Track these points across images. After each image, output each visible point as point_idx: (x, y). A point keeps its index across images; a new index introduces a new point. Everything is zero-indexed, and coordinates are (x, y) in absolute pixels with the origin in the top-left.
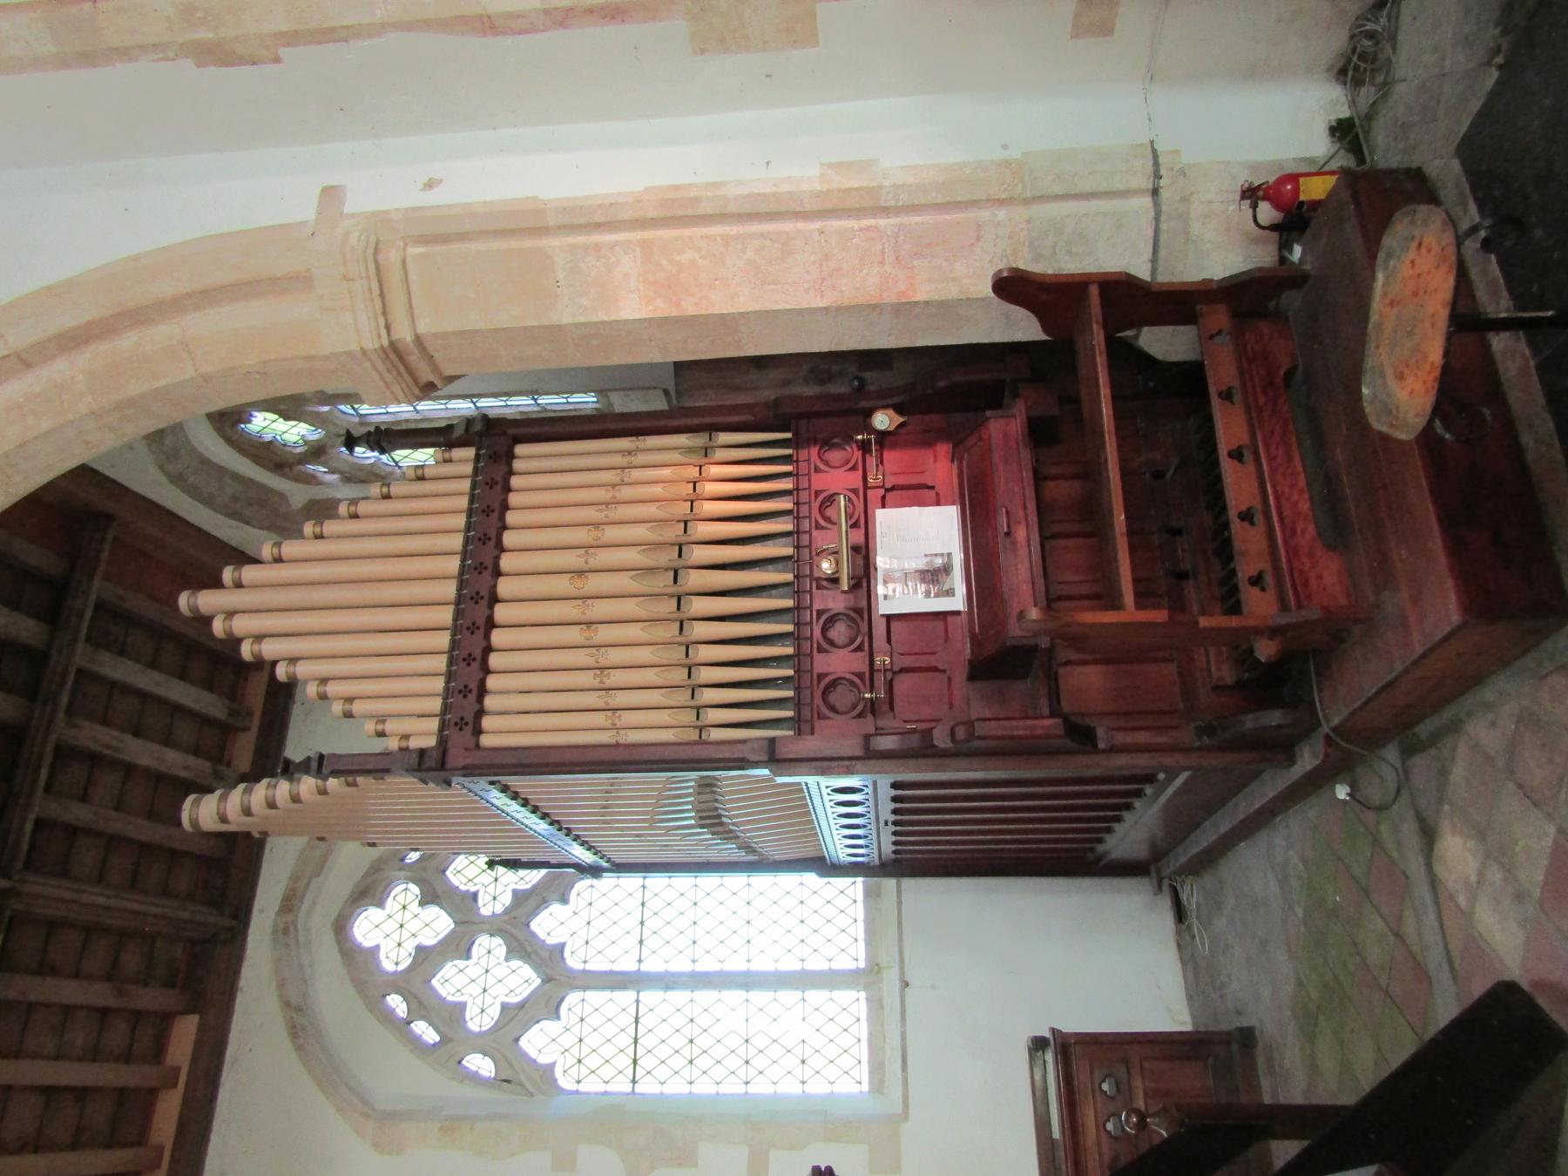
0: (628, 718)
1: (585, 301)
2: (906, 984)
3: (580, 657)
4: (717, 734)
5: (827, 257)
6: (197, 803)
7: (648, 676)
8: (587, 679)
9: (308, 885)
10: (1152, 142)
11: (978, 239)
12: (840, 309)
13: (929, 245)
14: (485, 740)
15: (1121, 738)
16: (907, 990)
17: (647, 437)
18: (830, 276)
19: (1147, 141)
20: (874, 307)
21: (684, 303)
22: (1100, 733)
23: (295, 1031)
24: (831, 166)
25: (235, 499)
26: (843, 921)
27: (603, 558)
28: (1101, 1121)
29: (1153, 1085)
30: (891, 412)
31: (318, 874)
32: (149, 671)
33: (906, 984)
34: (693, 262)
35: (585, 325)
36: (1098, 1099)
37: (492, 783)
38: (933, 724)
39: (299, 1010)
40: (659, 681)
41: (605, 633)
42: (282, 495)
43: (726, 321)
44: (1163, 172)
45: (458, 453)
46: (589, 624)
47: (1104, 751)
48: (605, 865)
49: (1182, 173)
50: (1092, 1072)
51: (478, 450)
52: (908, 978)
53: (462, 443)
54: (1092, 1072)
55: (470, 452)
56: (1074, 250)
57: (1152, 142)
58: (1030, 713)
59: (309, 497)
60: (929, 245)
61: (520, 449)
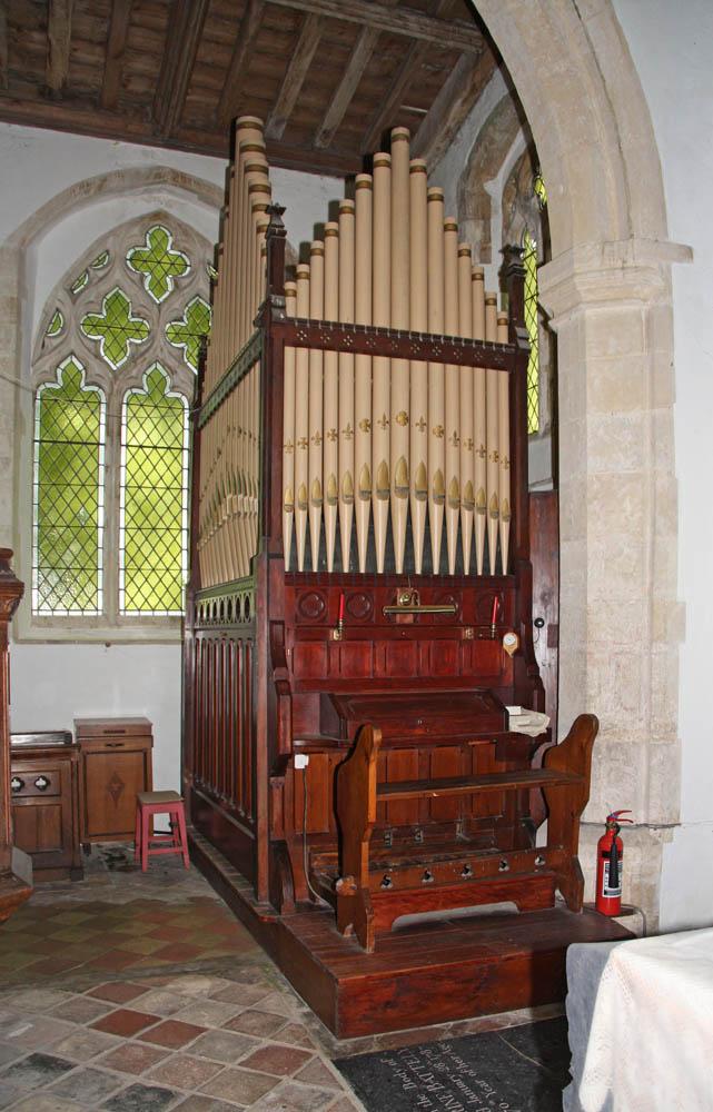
0: (301, 453)
1: (601, 432)
2: (108, 645)
3: (347, 419)
4: (287, 517)
5: (621, 605)
6: (257, 127)
7: (331, 469)
8: (331, 425)
9: (192, 191)
10: (679, 824)
11: (626, 709)
12: (586, 613)
13: (624, 677)
14: (289, 351)
15: (277, 793)
16: (104, 646)
17: (508, 470)
18: (608, 606)
19: (681, 821)
20: (585, 634)
21: (595, 502)
22: (281, 779)
23: (85, 186)
24: (683, 610)
25: (492, 141)
26: (153, 601)
27: (419, 436)
28: (19, 776)
29: (44, 811)
30: (516, 646)
31: (200, 199)
32: (361, 73)
33: (108, 645)
34: (624, 511)
35: (585, 431)
36: (33, 775)
37: (260, 353)
38: (290, 668)
39: (100, 187)
40: (327, 476)
41: (363, 437)
42: (494, 175)
43: (582, 535)
44: (658, 831)
45: (504, 330)
46: (371, 426)
47: (269, 780)
48: (201, 423)
49: (656, 843)
50: (52, 771)
51: (506, 346)
52: (112, 647)
53: (512, 335)
54: (52, 771)
55: (504, 340)
56: (613, 773)
57: (679, 824)
58: (294, 734)
59: (493, 196)
60: (624, 677)
61: (504, 375)
